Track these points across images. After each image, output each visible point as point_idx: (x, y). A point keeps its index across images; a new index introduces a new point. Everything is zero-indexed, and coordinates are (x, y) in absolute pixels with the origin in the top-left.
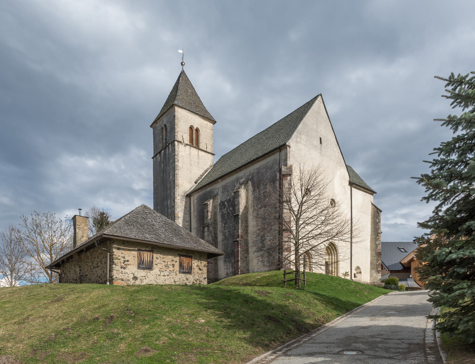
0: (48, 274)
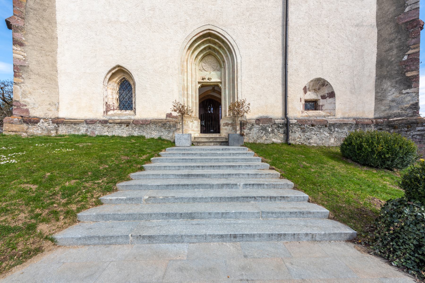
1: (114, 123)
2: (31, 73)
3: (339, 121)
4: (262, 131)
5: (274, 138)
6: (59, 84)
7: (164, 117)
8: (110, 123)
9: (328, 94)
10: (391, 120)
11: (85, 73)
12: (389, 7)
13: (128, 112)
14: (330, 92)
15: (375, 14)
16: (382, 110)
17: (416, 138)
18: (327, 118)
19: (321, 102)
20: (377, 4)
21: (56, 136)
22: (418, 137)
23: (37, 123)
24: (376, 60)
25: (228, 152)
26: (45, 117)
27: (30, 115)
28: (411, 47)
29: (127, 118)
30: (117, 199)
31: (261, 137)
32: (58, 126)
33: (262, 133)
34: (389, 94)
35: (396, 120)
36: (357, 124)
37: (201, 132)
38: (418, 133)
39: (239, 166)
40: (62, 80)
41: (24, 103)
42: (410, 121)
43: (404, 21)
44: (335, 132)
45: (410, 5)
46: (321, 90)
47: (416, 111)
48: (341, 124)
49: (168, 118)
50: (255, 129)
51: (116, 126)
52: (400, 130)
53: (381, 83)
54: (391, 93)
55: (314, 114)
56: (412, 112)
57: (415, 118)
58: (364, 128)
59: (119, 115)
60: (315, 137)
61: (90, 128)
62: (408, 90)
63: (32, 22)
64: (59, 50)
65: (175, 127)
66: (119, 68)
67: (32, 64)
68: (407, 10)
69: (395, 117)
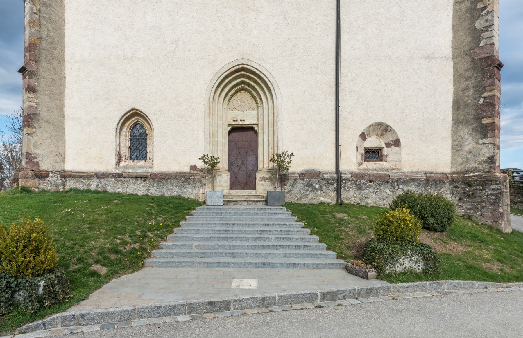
0: (409, 276)
1: (129, 177)
2: (42, 121)
3: (405, 176)
4: (307, 188)
5: (323, 197)
6: (66, 131)
7: (187, 169)
8: (125, 177)
9: (392, 141)
10: (467, 175)
12: (464, 38)
13: (142, 163)
14: (395, 139)
15: (451, 43)
16: (459, 163)
17: (490, 199)
18: (390, 171)
19: (386, 151)
20: (453, 31)
21: (63, 192)
22: (492, 197)
23: (47, 178)
24: (452, 100)
25: (263, 212)
26: (52, 170)
27: (40, 168)
28: (487, 88)
29: (143, 171)
30: (173, 245)
31: (307, 196)
32: (66, 181)
33: (307, 190)
34: (466, 143)
35: (472, 176)
36: (427, 180)
37: (231, 188)
38: (493, 192)
39: (274, 224)
40: (69, 126)
41: (35, 155)
42: (485, 178)
43: (479, 57)
44: (400, 190)
45: (485, 39)
47: (492, 165)
48: (406, 180)
49: (192, 172)
50: (300, 185)
51: (131, 181)
52: (475, 188)
53: (457, 129)
54: (468, 142)
55: (375, 166)
56: (488, 167)
57: (489, 174)
58: (436, 185)
59: (133, 167)
60: (374, 196)
61: (101, 183)
62: (485, 141)
63: (44, 64)
64: (67, 92)
65: (201, 183)
66: (134, 111)
67: (43, 112)
68: (482, 44)
69: (472, 172)
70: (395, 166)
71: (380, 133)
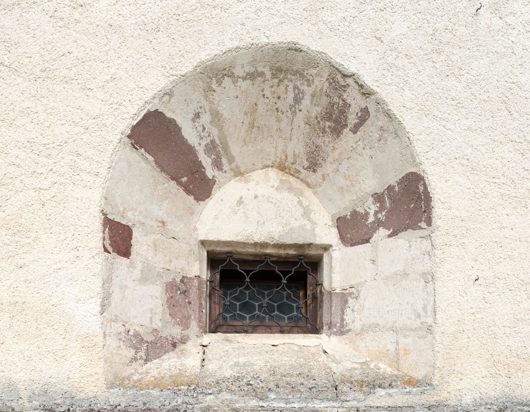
9: (378, 198)
11: (348, 159)
19: (340, 270)
46: (328, 168)
70: (396, 362)
71: (297, 147)
